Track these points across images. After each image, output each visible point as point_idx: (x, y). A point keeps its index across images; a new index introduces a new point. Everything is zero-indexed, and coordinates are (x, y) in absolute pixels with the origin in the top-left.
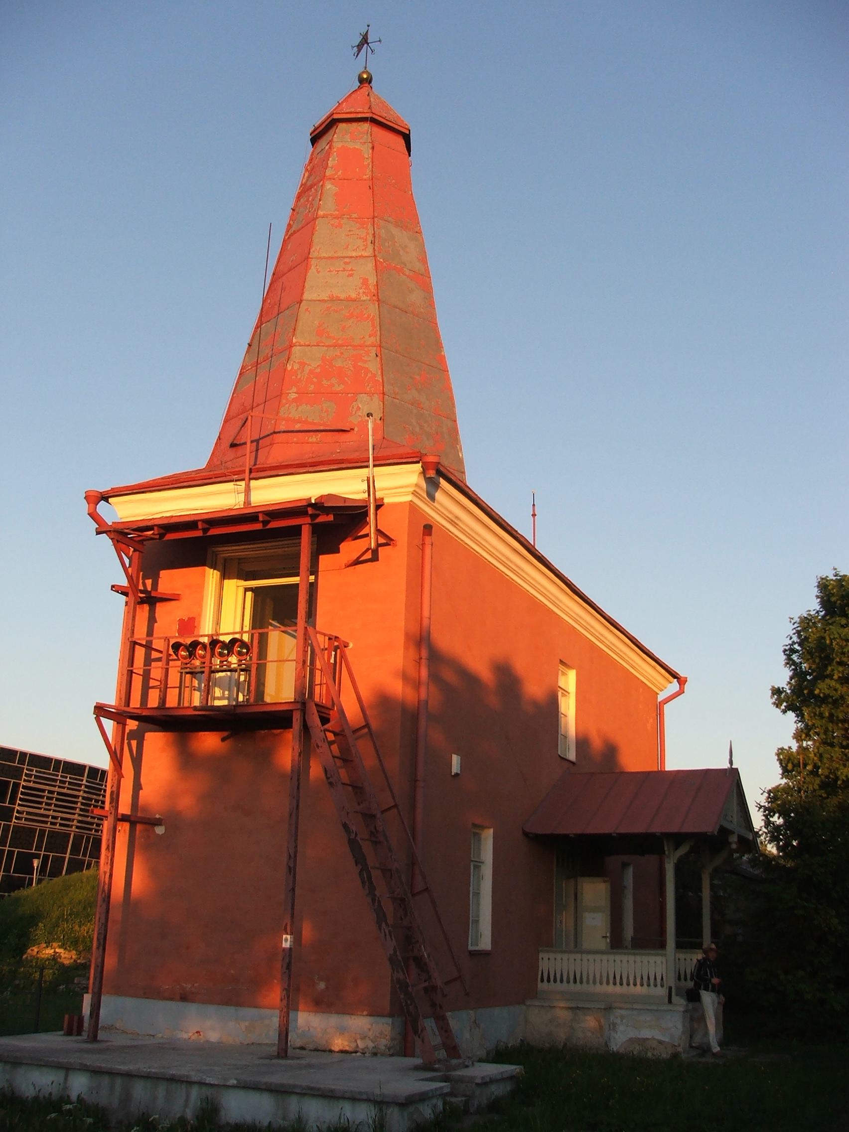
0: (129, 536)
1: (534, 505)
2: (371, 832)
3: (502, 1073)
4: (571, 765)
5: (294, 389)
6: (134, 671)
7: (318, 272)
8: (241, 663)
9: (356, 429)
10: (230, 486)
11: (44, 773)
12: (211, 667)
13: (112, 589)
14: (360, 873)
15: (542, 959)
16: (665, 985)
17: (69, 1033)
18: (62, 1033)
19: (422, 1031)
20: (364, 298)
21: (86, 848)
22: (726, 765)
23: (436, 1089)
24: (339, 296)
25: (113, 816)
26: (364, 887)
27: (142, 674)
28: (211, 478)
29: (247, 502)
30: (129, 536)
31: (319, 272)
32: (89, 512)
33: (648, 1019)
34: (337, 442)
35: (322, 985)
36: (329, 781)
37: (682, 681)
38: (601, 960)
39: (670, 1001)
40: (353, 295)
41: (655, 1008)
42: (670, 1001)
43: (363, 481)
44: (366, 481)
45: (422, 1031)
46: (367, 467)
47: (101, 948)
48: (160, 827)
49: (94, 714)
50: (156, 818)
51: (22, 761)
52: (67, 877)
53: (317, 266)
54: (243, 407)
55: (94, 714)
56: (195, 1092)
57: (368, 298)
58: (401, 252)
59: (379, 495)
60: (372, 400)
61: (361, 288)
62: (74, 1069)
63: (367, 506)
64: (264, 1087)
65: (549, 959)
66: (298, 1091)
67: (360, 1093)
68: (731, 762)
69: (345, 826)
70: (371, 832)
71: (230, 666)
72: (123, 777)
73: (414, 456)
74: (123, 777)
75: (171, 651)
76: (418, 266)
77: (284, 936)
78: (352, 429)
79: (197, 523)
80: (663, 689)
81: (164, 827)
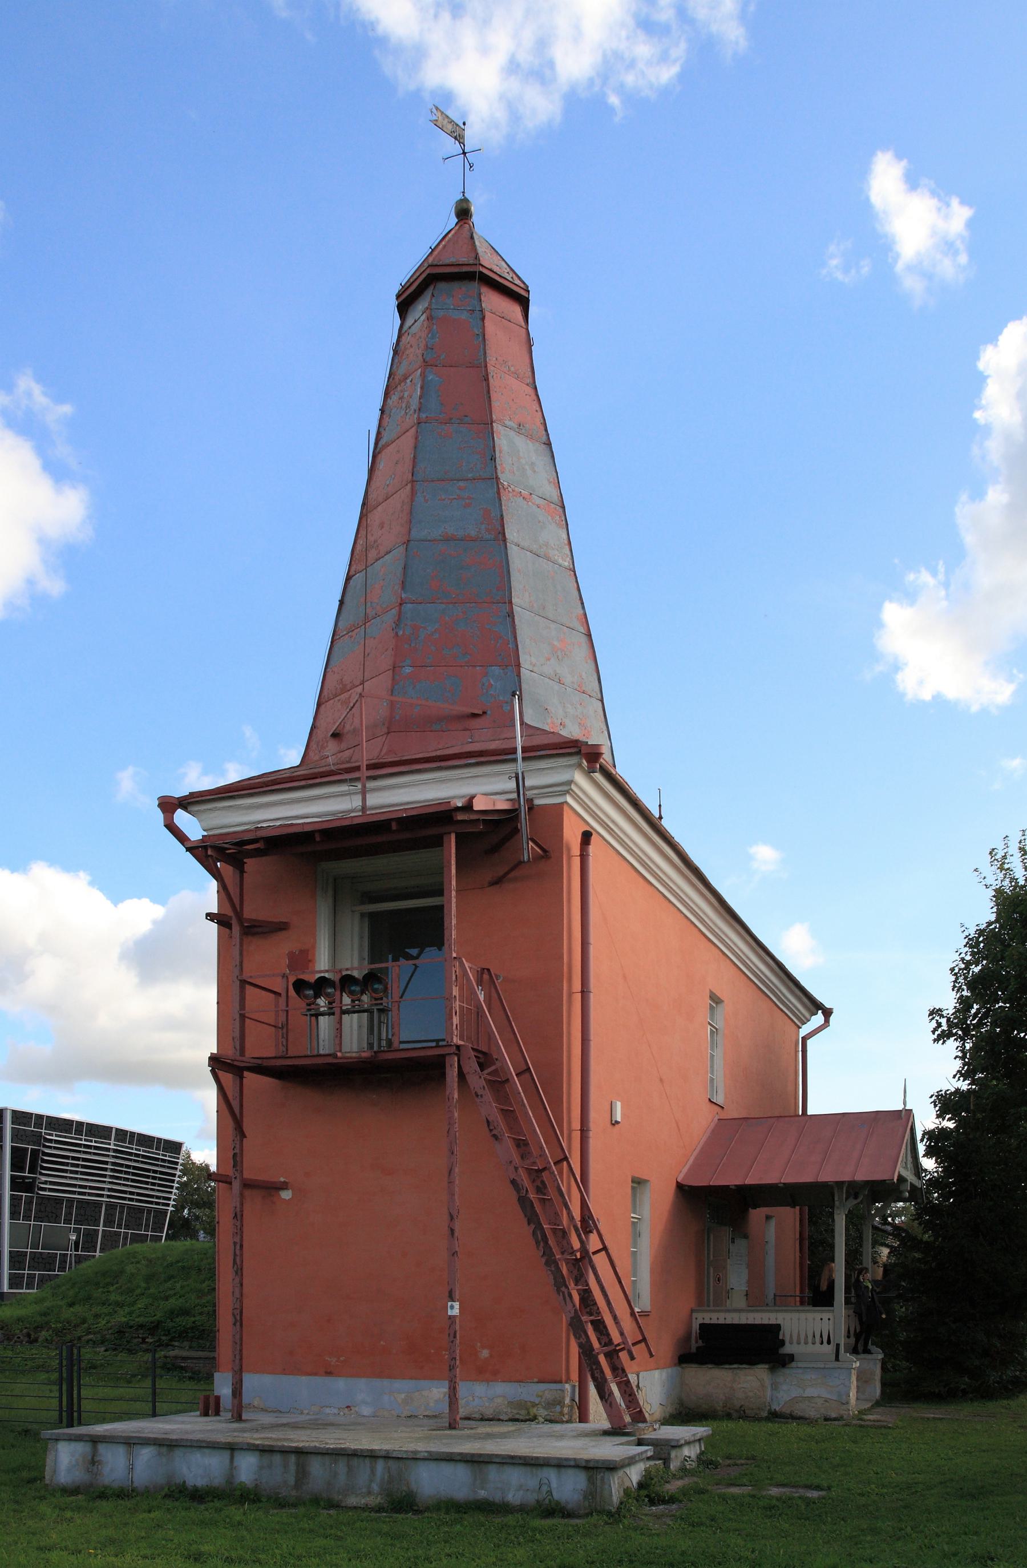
0: (227, 852)
1: (660, 806)
2: (537, 1187)
3: (694, 1435)
4: (719, 1109)
5: (408, 662)
6: (247, 1015)
7: (426, 501)
8: (354, 1004)
9: (489, 712)
10: (344, 788)
11: (65, 1137)
12: (341, 1007)
13: (207, 918)
14: (534, 1233)
15: (696, 1319)
16: (832, 1342)
17: (206, 1414)
18: (198, 1413)
19: (609, 1395)
20: (487, 536)
21: (121, 1219)
22: (900, 1107)
23: (642, 1453)
24: (456, 534)
25: (238, 1180)
26: (538, 1247)
27: (246, 1019)
28: (316, 778)
29: (364, 808)
30: (227, 852)
31: (428, 500)
32: (167, 823)
33: (813, 1377)
34: (468, 730)
35: (485, 1353)
36: (493, 1133)
37: (827, 1013)
38: (814, 1319)
39: (837, 1359)
40: (473, 533)
41: (822, 1366)
42: (837, 1359)
43: (510, 778)
44: (515, 779)
45: (609, 1395)
46: (515, 760)
47: (238, 1324)
48: (285, 1191)
49: (209, 1066)
50: (281, 1182)
51: (38, 1125)
52: (123, 1249)
53: (423, 492)
54: (341, 686)
55: (209, 1066)
56: (380, 1465)
57: (493, 536)
58: (529, 472)
59: (530, 794)
60: (506, 674)
61: (482, 523)
62: (242, 1449)
63: (516, 810)
64: (458, 1458)
65: (821, 1319)
66: (497, 1460)
67: (567, 1459)
68: (905, 1104)
69: (513, 1182)
70: (537, 1187)
71: (319, 1009)
72: (246, 1137)
73: (572, 745)
74: (246, 1137)
75: (292, 992)
76: (551, 492)
77: (449, 1304)
78: (484, 713)
79: (314, 835)
80: (805, 1021)
81: (290, 1191)
